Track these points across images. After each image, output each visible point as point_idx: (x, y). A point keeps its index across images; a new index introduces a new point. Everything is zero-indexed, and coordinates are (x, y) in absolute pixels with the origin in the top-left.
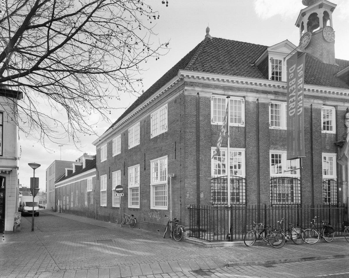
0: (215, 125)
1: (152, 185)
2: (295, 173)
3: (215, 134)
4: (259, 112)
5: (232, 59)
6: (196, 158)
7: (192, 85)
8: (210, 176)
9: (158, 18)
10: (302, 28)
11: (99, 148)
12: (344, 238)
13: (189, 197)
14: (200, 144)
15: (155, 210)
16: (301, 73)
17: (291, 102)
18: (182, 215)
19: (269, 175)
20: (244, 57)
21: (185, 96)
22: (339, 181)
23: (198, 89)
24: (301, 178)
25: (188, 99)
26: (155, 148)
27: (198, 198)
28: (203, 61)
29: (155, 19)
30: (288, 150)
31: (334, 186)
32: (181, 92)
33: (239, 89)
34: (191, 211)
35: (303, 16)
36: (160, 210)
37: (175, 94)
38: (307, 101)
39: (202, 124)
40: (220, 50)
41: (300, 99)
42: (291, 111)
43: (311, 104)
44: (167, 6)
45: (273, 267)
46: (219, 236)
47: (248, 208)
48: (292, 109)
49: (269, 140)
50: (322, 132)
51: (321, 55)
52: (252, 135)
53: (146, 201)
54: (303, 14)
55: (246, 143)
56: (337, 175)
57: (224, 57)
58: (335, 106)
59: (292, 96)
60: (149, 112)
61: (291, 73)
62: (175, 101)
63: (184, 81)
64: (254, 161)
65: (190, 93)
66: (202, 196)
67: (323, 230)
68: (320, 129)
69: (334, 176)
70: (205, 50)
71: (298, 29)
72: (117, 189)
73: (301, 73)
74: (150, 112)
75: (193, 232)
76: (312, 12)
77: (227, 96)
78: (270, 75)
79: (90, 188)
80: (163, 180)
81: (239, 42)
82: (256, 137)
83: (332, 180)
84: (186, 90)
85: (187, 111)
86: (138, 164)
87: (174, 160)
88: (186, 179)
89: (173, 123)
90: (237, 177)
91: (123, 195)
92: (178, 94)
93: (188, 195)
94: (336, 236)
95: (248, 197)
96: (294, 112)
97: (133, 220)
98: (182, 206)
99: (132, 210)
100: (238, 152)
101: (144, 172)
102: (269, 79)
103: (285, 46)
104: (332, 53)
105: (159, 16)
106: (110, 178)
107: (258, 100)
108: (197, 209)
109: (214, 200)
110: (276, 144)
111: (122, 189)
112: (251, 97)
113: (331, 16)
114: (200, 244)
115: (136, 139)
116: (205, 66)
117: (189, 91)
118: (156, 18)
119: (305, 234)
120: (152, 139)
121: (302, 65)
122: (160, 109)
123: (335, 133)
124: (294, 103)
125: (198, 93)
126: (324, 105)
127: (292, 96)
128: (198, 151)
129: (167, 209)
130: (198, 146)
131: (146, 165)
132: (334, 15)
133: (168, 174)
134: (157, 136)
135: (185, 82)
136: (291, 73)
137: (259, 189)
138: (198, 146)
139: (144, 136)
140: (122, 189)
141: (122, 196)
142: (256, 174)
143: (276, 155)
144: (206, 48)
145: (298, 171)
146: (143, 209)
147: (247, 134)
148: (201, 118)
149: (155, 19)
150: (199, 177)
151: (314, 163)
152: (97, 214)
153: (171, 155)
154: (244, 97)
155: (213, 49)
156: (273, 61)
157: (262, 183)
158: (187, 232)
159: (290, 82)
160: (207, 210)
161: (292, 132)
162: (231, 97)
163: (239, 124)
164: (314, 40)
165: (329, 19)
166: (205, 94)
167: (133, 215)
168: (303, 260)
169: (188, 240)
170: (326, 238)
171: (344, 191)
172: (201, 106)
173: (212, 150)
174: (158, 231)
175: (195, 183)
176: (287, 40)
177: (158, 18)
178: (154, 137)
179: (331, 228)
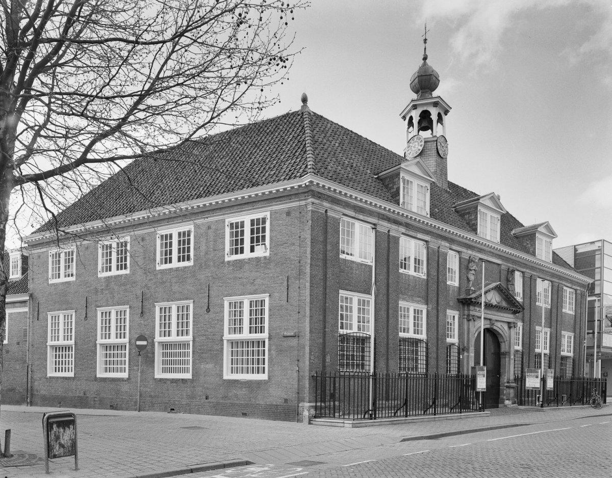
7: (320, 197)
31: (454, 352)
33: (371, 213)
37: (287, 203)
38: (436, 240)
39: (329, 254)
56: (459, 339)
58: (459, 252)
66: (328, 359)
76: (425, 108)
83: (453, 344)
87: (284, 303)
99: (169, 382)
101: (207, 316)
107: (389, 231)
112: (384, 226)
125: (326, 211)
126: (450, 249)
129: (267, 379)
148: (329, 247)
150: (325, 331)
156: (404, 180)
160: (330, 378)
175: (321, 340)
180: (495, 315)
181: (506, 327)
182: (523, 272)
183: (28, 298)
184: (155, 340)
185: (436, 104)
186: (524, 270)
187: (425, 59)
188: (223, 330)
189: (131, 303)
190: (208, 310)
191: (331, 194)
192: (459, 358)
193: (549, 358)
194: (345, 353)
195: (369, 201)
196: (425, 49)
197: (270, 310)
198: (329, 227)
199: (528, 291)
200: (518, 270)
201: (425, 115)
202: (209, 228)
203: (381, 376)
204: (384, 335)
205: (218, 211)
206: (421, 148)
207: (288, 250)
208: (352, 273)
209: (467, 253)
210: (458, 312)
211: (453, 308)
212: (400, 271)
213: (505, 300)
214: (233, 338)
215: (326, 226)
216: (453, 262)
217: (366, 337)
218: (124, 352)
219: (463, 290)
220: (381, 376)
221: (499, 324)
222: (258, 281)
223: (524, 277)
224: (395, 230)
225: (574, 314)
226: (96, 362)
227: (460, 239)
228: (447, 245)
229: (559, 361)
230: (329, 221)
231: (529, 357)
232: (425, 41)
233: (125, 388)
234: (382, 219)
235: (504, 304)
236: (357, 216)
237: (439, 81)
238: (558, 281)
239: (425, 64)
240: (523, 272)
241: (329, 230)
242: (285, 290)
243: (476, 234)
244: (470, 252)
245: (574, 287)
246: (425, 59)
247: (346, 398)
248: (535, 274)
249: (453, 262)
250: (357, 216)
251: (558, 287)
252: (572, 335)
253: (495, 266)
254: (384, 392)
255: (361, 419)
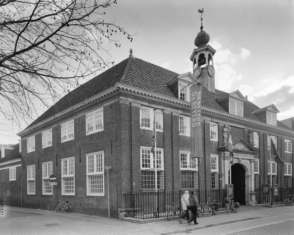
0: (143, 129)
1: (88, 175)
2: (195, 168)
3: (143, 136)
4: (172, 123)
5: (152, 79)
6: (129, 154)
7: (126, 96)
8: (140, 169)
9: (120, 47)
10: (195, 62)
11: (24, 139)
12: (225, 211)
13: (124, 185)
14: (132, 144)
15: (92, 197)
16: (199, 98)
17: (194, 118)
18: (118, 200)
19: (180, 169)
20: (160, 78)
21: (120, 104)
22: (220, 174)
23: (130, 100)
24: (198, 172)
25: (123, 107)
26: (90, 144)
27: (131, 186)
28: (132, 77)
29: (117, 46)
30: (191, 151)
32: (117, 100)
34: (127, 197)
35: (196, 54)
36: (96, 197)
37: (111, 101)
39: (133, 127)
40: (142, 69)
41: (195, 116)
42: (193, 124)
43: (204, 120)
44: (131, 41)
45: (191, 233)
46: (147, 215)
47: (166, 193)
48: (194, 122)
49: (179, 143)
50: (211, 140)
51: (207, 85)
52: (168, 139)
53: (81, 189)
54: (195, 53)
55: (164, 145)
57: (146, 76)
58: (217, 123)
59: (194, 114)
60: (84, 112)
61: (193, 97)
62: (111, 106)
63: (119, 92)
64: (169, 158)
65: (124, 102)
66: (134, 184)
67: (214, 207)
68: (210, 138)
69: (217, 170)
70: (132, 68)
71: (192, 63)
72: (51, 179)
73: (199, 98)
74: (85, 112)
75: (128, 213)
76: (201, 53)
77: (154, 109)
78: (179, 96)
79: (13, 178)
80: (99, 171)
81: (155, 65)
82: (170, 140)
83: (216, 173)
84: (121, 99)
85: (122, 116)
86: (72, 156)
87: (110, 155)
88: (122, 171)
89: (109, 124)
90: (159, 170)
91: (57, 184)
92: (113, 102)
93: (124, 184)
94: (221, 210)
95: (166, 185)
96: (196, 125)
97: (69, 206)
98: (119, 192)
99: (66, 197)
100: (147, 150)
101: (80, 164)
102: (179, 99)
103: (188, 76)
104: (213, 84)
105: (120, 45)
106: (39, 168)
107: (172, 113)
108: (130, 195)
109: (142, 187)
110: (183, 147)
111: (55, 178)
112: (168, 111)
113: (213, 58)
114: (136, 221)
115: (49, 134)
116: (134, 81)
117: (124, 101)
118: (118, 46)
119: (204, 210)
120: (88, 136)
121: (200, 92)
122: (96, 111)
123: (218, 141)
124: (196, 118)
125: (130, 103)
126: (212, 121)
127: (194, 114)
128: (131, 149)
129: (104, 196)
130: (131, 145)
131: (81, 158)
132: (214, 57)
133: (104, 166)
134: (93, 134)
135: (120, 93)
136: (193, 97)
137: (173, 179)
138: (131, 145)
139: (79, 133)
140: (55, 178)
141: (55, 184)
142: (171, 168)
143: (184, 155)
144: (132, 66)
145: (197, 167)
146: (79, 196)
147: (165, 138)
148: (133, 123)
149: (117, 46)
150: (132, 169)
151: (206, 161)
152: (23, 202)
153: (107, 151)
154: (163, 110)
155: (137, 67)
157: (175, 175)
158: (124, 213)
159: (193, 103)
161: (194, 138)
162: (157, 110)
163: (160, 130)
164: (202, 73)
165: (211, 60)
166: (136, 104)
167: (67, 202)
168: (207, 227)
169: (125, 219)
170: (215, 212)
171: (223, 181)
172: (132, 113)
173: (141, 149)
174: (95, 214)
175: (129, 174)
176: (190, 72)
177: (120, 47)
178: (90, 135)
179: (218, 205)
180: (241, 156)
181: (248, 162)
182: (259, 132)
183: (21, 160)
184: (62, 177)
185: (207, 50)
186: (259, 131)
187: (202, 28)
188: (86, 170)
189: (53, 160)
190: (80, 161)
191: (133, 94)
192: (219, 180)
193: (277, 178)
194: (192, 180)
195: (166, 99)
196: (202, 23)
197: (104, 159)
198: (132, 112)
199: (262, 142)
200: (255, 131)
201: (202, 57)
202: (80, 120)
203: (202, 192)
204: (170, 169)
205: (82, 111)
206: (200, 73)
207: (111, 126)
208: (148, 137)
209: (222, 123)
210: (218, 155)
211: (214, 153)
212: (180, 134)
213: (247, 147)
214: (92, 175)
215: (131, 111)
216: (214, 129)
217: (160, 171)
218: (102, 184)
219: (221, 143)
220: (202, 192)
221: (244, 161)
222: (99, 145)
223: (259, 135)
224: (176, 113)
225: (292, 153)
226: (42, 188)
227: (216, 115)
228: (210, 119)
229: (283, 179)
230: (132, 109)
231: (264, 177)
232: (202, 19)
233: (51, 200)
234: (167, 106)
235: (247, 150)
236: (151, 105)
237: (209, 38)
238: (281, 136)
239: (202, 31)
240: (259, 132)
241: (133, 114)
242: (111, 148)
243: (228, 112)
244: (224, 123)
245: (291, 139)
246: (202, 28)
247: (147, 205)
248: (266, 132)
249: (214, 129)
250: (151, 105)
251: (281, 139)
252: (291, 164)
253: (241, 130)
254: (204, 198)
255: (141, 218)
